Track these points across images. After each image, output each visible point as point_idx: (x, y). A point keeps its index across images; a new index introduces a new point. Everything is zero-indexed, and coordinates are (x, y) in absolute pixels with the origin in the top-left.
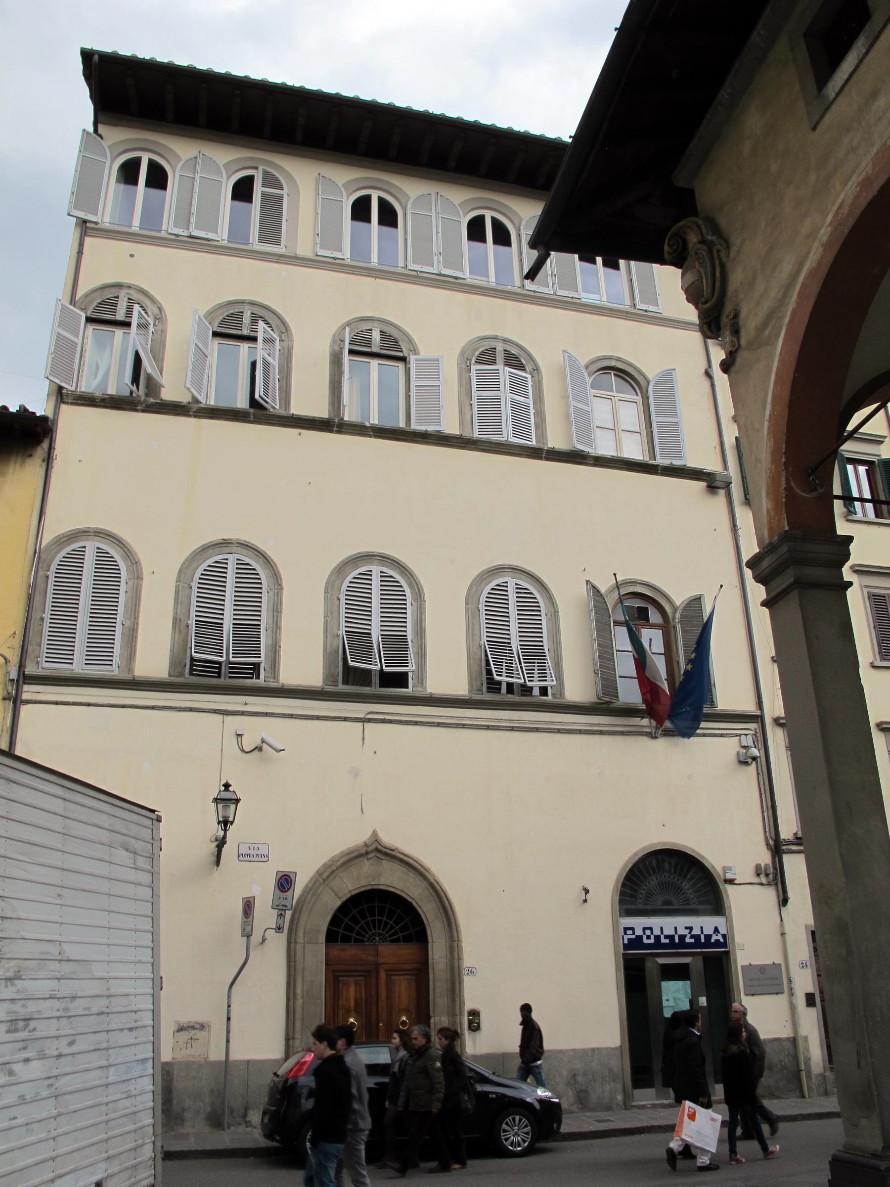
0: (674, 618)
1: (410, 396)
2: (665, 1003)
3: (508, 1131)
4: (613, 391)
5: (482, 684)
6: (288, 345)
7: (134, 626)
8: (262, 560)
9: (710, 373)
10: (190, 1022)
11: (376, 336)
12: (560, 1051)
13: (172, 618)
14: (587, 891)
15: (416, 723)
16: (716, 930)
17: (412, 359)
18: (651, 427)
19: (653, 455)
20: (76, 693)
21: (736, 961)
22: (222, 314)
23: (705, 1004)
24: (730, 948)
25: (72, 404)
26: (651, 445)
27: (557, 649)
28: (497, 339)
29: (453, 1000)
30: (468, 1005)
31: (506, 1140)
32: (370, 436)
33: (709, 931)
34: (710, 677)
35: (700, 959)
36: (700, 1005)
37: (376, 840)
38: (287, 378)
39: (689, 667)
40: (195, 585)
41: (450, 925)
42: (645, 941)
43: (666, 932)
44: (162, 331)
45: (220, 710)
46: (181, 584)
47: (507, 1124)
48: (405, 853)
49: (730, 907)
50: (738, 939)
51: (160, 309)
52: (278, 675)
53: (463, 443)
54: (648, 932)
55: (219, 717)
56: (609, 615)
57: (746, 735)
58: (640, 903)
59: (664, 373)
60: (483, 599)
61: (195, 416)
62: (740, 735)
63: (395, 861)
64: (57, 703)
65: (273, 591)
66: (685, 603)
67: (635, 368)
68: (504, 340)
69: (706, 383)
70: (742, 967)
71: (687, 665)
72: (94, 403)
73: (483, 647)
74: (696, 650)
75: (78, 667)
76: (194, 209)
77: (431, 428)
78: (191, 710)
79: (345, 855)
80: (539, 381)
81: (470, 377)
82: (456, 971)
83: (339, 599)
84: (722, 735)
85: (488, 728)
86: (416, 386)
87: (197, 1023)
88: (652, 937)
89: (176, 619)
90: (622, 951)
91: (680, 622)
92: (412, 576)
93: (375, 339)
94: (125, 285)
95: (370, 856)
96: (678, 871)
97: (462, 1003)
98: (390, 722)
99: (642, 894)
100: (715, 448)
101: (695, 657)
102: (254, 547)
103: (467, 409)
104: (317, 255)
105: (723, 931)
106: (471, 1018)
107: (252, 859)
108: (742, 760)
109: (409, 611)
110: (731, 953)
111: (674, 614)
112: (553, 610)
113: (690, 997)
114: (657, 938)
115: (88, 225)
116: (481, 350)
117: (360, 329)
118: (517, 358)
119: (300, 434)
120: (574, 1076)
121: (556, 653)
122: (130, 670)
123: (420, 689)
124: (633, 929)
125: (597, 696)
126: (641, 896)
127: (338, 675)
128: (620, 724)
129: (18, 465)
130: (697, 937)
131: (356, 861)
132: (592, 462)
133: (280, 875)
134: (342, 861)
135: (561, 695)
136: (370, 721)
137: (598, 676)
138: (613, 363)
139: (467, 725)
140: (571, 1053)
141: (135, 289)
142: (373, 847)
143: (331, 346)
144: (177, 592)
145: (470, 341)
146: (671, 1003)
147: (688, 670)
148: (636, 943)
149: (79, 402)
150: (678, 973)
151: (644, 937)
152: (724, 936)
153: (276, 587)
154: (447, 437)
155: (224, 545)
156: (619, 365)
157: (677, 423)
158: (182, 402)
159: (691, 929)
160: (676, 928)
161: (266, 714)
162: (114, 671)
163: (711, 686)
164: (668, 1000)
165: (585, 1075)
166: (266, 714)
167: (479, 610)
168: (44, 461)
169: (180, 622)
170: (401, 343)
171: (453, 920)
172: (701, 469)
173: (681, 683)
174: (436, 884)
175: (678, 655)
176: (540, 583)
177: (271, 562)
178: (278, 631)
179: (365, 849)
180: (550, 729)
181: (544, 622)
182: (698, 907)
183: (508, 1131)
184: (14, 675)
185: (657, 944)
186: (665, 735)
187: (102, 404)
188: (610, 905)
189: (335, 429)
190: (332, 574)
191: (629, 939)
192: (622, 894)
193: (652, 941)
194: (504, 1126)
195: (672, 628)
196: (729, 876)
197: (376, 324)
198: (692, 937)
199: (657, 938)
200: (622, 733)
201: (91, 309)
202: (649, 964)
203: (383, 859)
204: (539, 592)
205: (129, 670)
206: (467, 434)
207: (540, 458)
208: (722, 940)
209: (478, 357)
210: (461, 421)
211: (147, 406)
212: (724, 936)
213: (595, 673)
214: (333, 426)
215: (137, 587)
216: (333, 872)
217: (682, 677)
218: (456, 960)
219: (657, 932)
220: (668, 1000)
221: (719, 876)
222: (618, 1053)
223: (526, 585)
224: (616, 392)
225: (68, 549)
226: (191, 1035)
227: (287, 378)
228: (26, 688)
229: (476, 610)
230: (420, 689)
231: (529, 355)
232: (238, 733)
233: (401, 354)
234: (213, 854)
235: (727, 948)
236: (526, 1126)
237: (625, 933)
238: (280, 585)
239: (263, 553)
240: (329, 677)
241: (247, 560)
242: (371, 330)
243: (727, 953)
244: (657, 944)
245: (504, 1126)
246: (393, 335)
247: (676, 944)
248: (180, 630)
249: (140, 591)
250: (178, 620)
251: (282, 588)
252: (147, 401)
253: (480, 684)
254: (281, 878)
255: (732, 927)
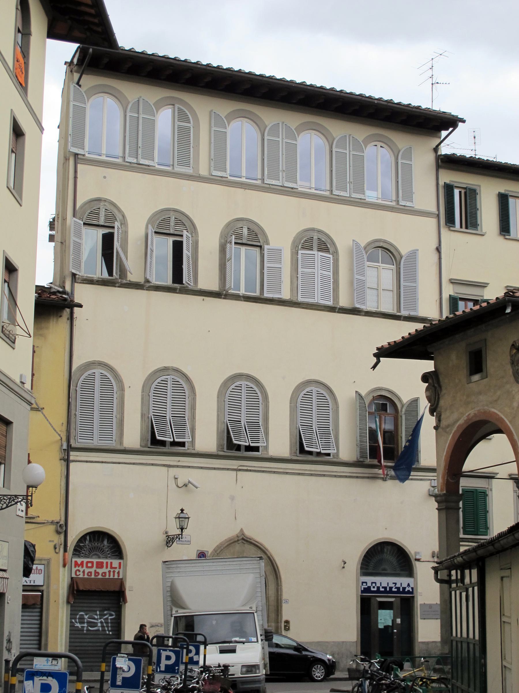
0: (401, 411)
1: (263, 273)
2: (379, 621)
3: (315, 671)
4: (379, 263)
5: (297, 450)
6: (196, 239)
7: (122, 418)
8: (185, 379)
9: (439, 249)
10: (156, 623)
11: (245, 231)
12: (327, 642)
13: (140, 413)
14: (345, 563)
15: (263, 471)
16: (409, 585)
17: (266, 247)
18: (400, 288)
19: (399, 310)
20: (95, 456)
21: (417, 601)
22: (158, 219)
23: (400, 622)
24: (415, 594)
25: (80, 283)
26: (398, 301)
27: (337, 430)
28: (314, 230)
29: (278, 615)
30: (284, 618)
31: (314, 675)
32: (241, 300)
33: (405, 585)
34: (418, 445)
35: (399, 600)
36: (397, 623)
37: (243, 534)
38: (196, 262)
39: (407, 444)
40: (151, 394)
41: (277, 578)
42: (372, 589)
43: (383, 585)
44: (125, 232)
45: (167, 465)
46: (144, 393)
47: (315, 668)
48: (257, 541)
49: (417, 573)
50: (420, 590)
51: (124, 216)
52: (195, 446)
53: (292, 304)
54: (374, 585)
55: (165, 469)
56: (366, 410)
57: (434, 480)
58: (370, 569)
59: (411, 253)
60: (299, 400)
61: (147, 290)
62: (431, 480)
63: (252, 545)
64: (87, 462)
65: (191, 397)
66: (409, 402)
67: (394, 247)
68: (319, 231)
69: (436, 256)
70: (421, 605)
71: (407, 442)
72: (93, 283)
73: (298, 429)
74: (412, 435)
75: (96, 442)
76: (140, 144)
77: (276, 296)
78: (152, 465)
79: (227, 542)
80: (337, 259)
81: (298, 258)
82: (280, 601)
83: (224, 401)
84: (421, 480)
85: (299, 474)
86: (268, 267)
87: (159, 623)
88: (376, 587)
89: (143, 414)
90: (360, 594)
91: (405, 414)
92: (262, 387)
93: (245, 234)
94: (102, 199)
95: (239, 542)
96: (394, 554)
97: (281, 616)
98: (250, 471)
99: (372, 564)
100: (436, 301)
101: (411, 439)
102: (181, 371)
103: (295, 280)
104: (212, 175)
105: (412, 585)
106: (285, 624)
107: (183, 543)
108: (431, 494)
109: (261, 408)
110: (415, 597)
111: (402, 408)
112: (336, 407)
113: (392, 618)
114: (378, 588)
115: (79, 156)
116: (304, 239)
117: (236, 227)
118: (325, 244)
119: (203, 300)
120: (333, 654)
121: (336, 431)
122: (121, 443)
123: (265, 453)
124: (366, 583)
125: (357, 458)
126: (371, 565)
127: (224, 445)
128: (366, 472)
129: (54, 322)
130: (398, 588)
131: (233, 545)
132: (364, 314)
133: (199, 552)
134: (226, 544)
135: (337, 456)
136: (240, 470)
137: (358, 447)
138: (381, 244)
139: (288, 472)
140: (332, 643)
141: (108, 202)
142: (241, 537)
143: (219, 240)
144: (142, 399)
145: (299, 232)
146: (383, 621)
147: (407, 446)
148: (367, 590)
149: (84, 282)
150: (384, 606)
151: (372, 587)
152: (412, 588)
153: (193, 395)
154: (284, 301)
155: (165, 370)
156: (385, 245)
157: (416, 287)
158: (141, 282)
159: (396, 584)
160: (388, 583)
161: (189, 467)
162: (113, 444)
163: (418, 452)
164: (381, 620)
165: (338, 654)
166: (189, 467)
167: (297, 407)
168: (68, 319)
169: (145, 416)
170: (259, 236)
171: (279, 576)
172: (426, 317)
173: (402, 452)
174: (271, 557)
175: (402, 433)
176: (330, 390)
177: (190, 380)
178: (194, 420)
179: (237, 538)
180: (331, 475)
181: (331, 414)
182: (400, 572)
183: (315, 671)
184: (65, 447)
185: (378, 591)
186: (391, 479)
187: (97, 283)
188: (356, 570)
189: (223, 297)
190: (221, 387)
191: (364, 588)
192: (362, 564)
193: (375, 589)
194: (314, 669)
195: (400, 417)
196: (418, 557)
197: (245, 222)
198: (396, 588)
199: (378, 588)
200: (368, 478)
201: (85, 217)
202: (373, 601)
203: (245, 544)
204: (329, 395)
205: (121, 443)
206: (294, 300)
207: (335, 312)
208: (411, 590)
209: (303, 244)
210: (291, 289)
211: (121, 284)
212: (412, 588)
213: (357, 445)
214: (222, 295)
215: (122, 396)
216: (222, 550)
217: (403, 449)
218: (280, 596)
219: (378, 585)
220: (381, 620)
221: (412, 556)
222: (355, 644)
223: (322, 392)
224: (381, 263)
225: (86, 374)
226: (157, 629)
227: (196, 262)
228: (72, 453)
229: (295, 407)
230: (265, 453)
231: (332, 241)
232: (176, 477)
233: (259, 244)
234: (165, 540)
235: (413, 594)
236: (322, 670)
237: (362, 585)
238: (195, 394)
239: (185, 375)
240: (220, 447)
241: (178, 379)
242: (242, 227)
243: (413, 597)
244: (378, 591)
245: (314, 669)
246: (254, 231)
247: (388, 591)
248: (145, 420)
249: (124, 398)
250: (144, 414)
251: (196, 396)
252: (122, 282)
253: (296, 449)
254: (200, 553)
255: (417, 584)
